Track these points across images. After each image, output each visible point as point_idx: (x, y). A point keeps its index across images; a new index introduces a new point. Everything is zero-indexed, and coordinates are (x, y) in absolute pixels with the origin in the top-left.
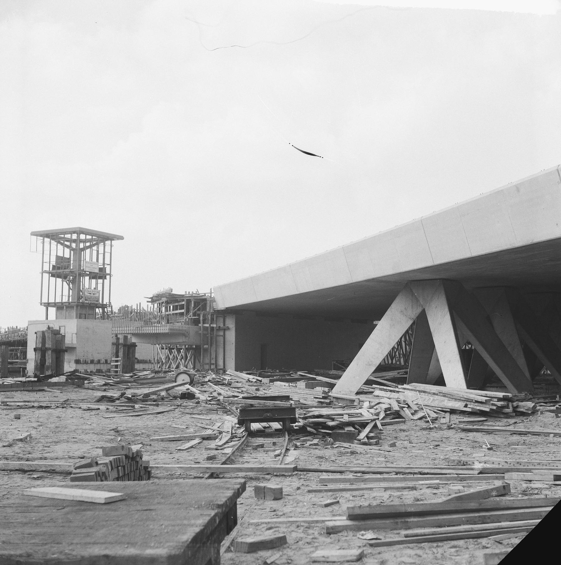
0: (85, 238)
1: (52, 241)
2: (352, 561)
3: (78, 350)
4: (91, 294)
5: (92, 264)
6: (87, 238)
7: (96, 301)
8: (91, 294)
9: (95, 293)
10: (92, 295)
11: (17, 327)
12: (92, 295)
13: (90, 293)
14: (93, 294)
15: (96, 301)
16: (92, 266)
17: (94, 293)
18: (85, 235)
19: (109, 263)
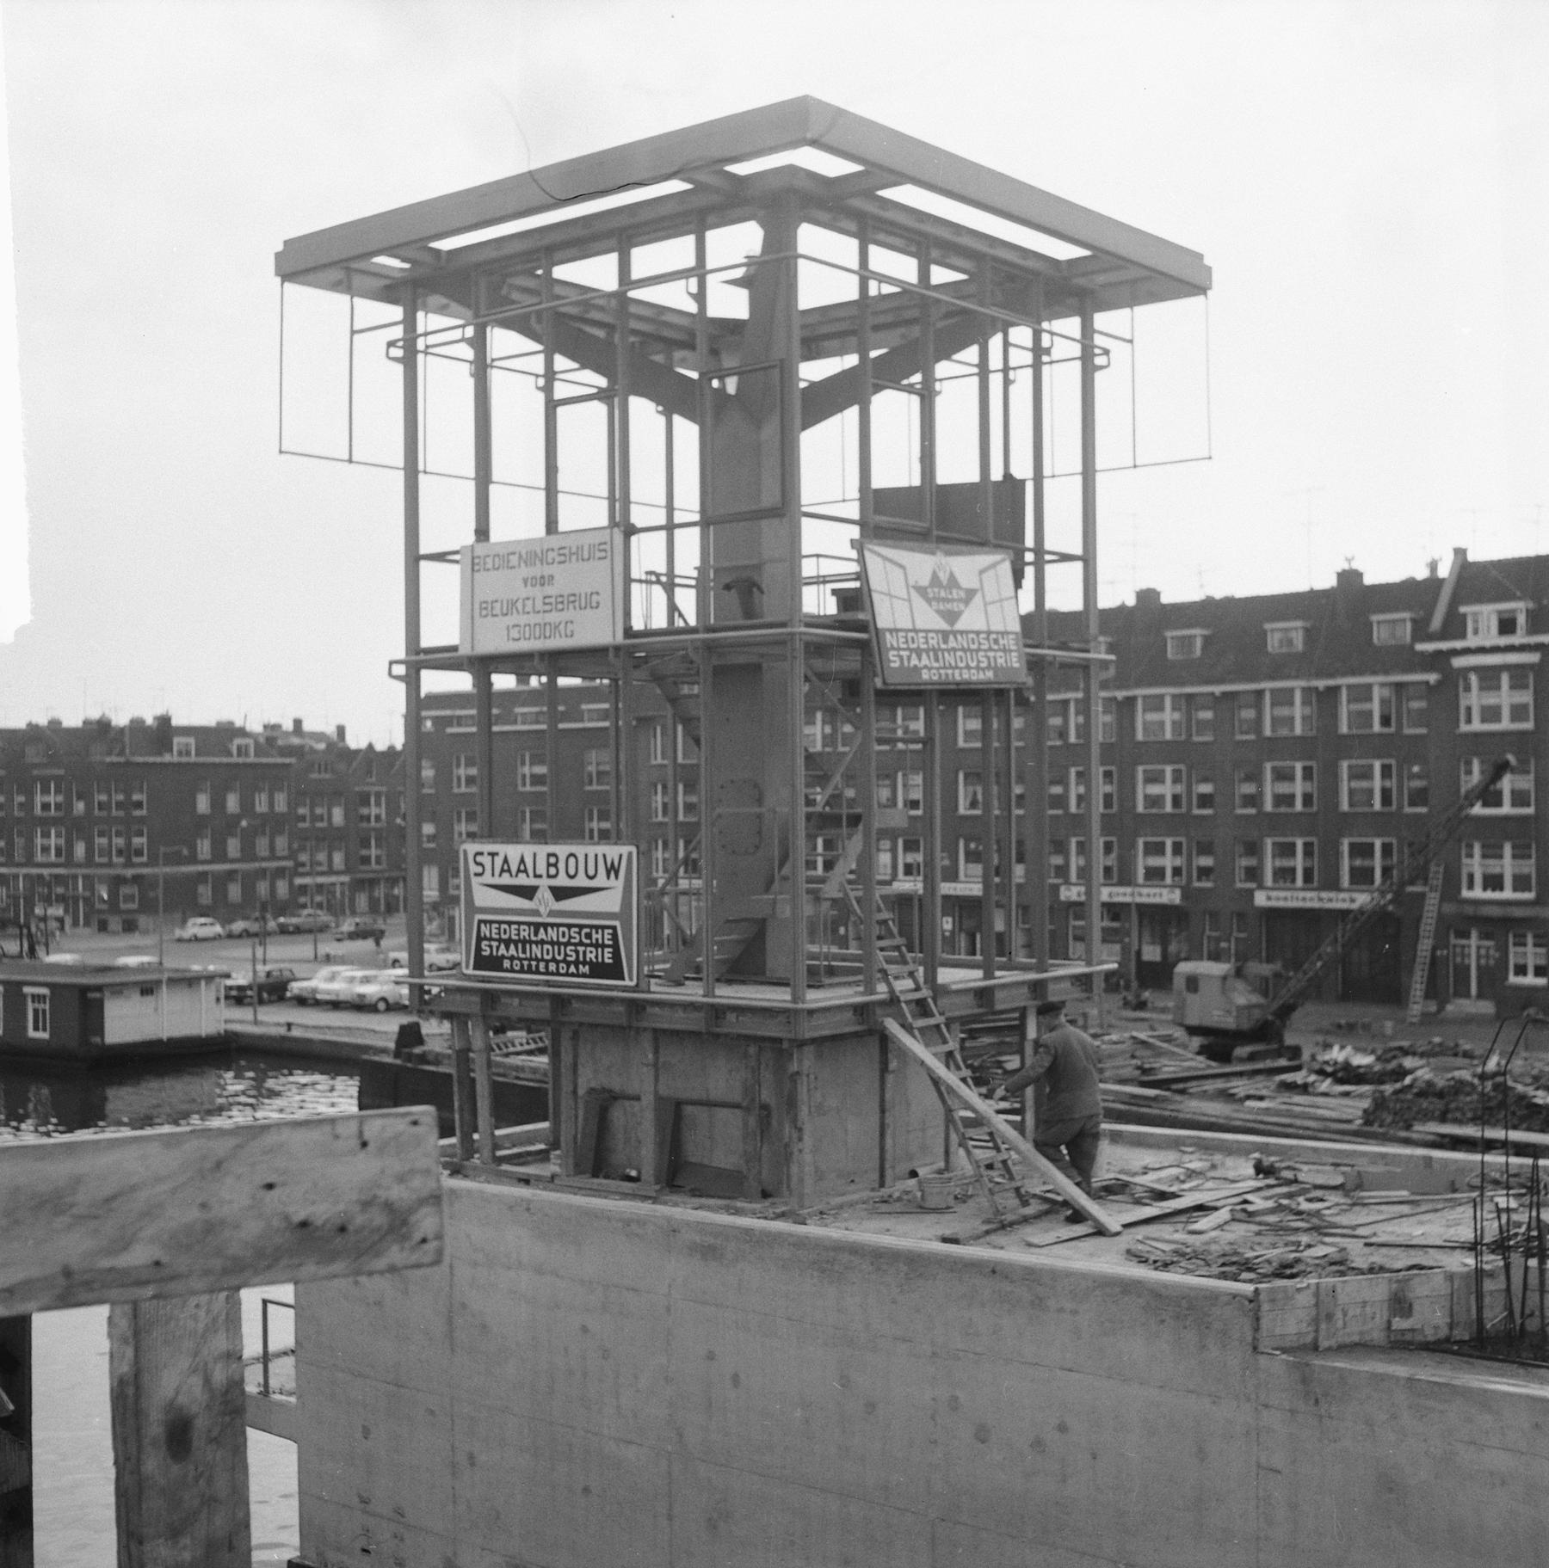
0: (292, 1311)
1: (503, 341)
2: (905, 574)
3: (460, 648)
4: (528, 892)
5: (537, 570)
6: (690, 240)
7: (598, 970)
8: (528, 892)
9: (581, 881)
10: (544, 902)
11: (298, 723)
12: (544, 902)
13: (522, 880)
14: (560, 893)
15: (598, 970)
16: (543, 581)
17: (562, 881)
18: (423, 564)
19: (1077, 550)
